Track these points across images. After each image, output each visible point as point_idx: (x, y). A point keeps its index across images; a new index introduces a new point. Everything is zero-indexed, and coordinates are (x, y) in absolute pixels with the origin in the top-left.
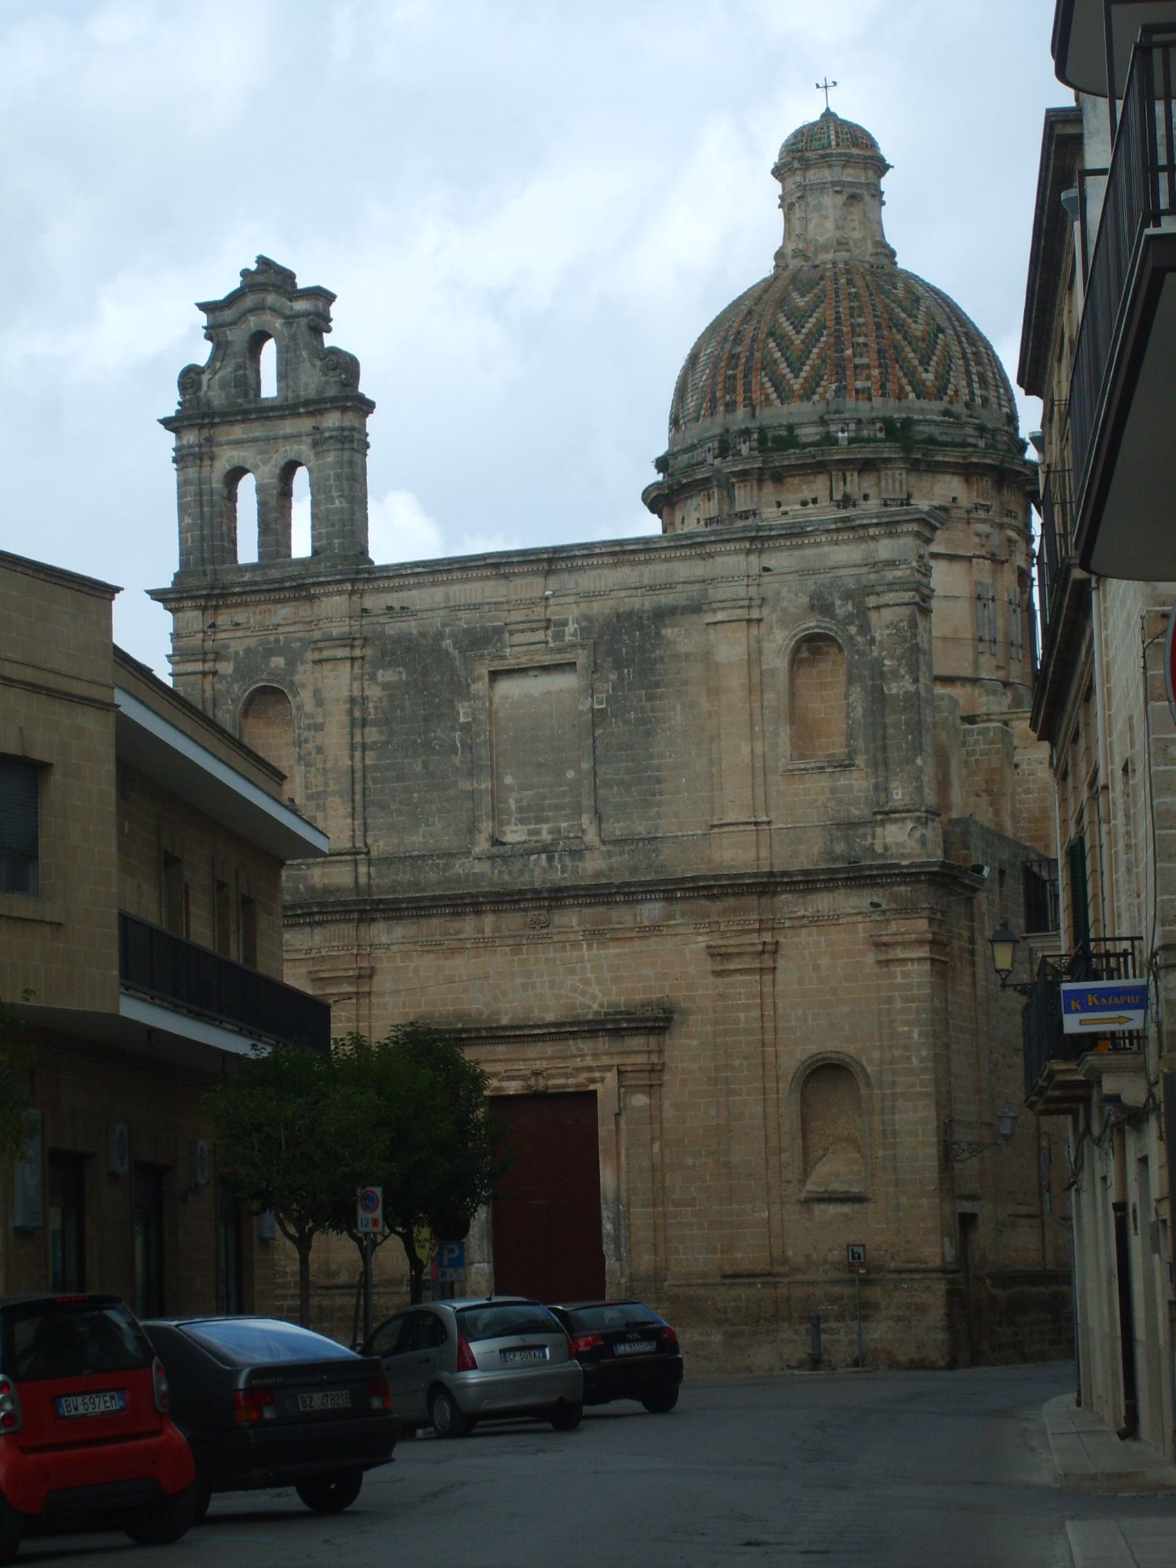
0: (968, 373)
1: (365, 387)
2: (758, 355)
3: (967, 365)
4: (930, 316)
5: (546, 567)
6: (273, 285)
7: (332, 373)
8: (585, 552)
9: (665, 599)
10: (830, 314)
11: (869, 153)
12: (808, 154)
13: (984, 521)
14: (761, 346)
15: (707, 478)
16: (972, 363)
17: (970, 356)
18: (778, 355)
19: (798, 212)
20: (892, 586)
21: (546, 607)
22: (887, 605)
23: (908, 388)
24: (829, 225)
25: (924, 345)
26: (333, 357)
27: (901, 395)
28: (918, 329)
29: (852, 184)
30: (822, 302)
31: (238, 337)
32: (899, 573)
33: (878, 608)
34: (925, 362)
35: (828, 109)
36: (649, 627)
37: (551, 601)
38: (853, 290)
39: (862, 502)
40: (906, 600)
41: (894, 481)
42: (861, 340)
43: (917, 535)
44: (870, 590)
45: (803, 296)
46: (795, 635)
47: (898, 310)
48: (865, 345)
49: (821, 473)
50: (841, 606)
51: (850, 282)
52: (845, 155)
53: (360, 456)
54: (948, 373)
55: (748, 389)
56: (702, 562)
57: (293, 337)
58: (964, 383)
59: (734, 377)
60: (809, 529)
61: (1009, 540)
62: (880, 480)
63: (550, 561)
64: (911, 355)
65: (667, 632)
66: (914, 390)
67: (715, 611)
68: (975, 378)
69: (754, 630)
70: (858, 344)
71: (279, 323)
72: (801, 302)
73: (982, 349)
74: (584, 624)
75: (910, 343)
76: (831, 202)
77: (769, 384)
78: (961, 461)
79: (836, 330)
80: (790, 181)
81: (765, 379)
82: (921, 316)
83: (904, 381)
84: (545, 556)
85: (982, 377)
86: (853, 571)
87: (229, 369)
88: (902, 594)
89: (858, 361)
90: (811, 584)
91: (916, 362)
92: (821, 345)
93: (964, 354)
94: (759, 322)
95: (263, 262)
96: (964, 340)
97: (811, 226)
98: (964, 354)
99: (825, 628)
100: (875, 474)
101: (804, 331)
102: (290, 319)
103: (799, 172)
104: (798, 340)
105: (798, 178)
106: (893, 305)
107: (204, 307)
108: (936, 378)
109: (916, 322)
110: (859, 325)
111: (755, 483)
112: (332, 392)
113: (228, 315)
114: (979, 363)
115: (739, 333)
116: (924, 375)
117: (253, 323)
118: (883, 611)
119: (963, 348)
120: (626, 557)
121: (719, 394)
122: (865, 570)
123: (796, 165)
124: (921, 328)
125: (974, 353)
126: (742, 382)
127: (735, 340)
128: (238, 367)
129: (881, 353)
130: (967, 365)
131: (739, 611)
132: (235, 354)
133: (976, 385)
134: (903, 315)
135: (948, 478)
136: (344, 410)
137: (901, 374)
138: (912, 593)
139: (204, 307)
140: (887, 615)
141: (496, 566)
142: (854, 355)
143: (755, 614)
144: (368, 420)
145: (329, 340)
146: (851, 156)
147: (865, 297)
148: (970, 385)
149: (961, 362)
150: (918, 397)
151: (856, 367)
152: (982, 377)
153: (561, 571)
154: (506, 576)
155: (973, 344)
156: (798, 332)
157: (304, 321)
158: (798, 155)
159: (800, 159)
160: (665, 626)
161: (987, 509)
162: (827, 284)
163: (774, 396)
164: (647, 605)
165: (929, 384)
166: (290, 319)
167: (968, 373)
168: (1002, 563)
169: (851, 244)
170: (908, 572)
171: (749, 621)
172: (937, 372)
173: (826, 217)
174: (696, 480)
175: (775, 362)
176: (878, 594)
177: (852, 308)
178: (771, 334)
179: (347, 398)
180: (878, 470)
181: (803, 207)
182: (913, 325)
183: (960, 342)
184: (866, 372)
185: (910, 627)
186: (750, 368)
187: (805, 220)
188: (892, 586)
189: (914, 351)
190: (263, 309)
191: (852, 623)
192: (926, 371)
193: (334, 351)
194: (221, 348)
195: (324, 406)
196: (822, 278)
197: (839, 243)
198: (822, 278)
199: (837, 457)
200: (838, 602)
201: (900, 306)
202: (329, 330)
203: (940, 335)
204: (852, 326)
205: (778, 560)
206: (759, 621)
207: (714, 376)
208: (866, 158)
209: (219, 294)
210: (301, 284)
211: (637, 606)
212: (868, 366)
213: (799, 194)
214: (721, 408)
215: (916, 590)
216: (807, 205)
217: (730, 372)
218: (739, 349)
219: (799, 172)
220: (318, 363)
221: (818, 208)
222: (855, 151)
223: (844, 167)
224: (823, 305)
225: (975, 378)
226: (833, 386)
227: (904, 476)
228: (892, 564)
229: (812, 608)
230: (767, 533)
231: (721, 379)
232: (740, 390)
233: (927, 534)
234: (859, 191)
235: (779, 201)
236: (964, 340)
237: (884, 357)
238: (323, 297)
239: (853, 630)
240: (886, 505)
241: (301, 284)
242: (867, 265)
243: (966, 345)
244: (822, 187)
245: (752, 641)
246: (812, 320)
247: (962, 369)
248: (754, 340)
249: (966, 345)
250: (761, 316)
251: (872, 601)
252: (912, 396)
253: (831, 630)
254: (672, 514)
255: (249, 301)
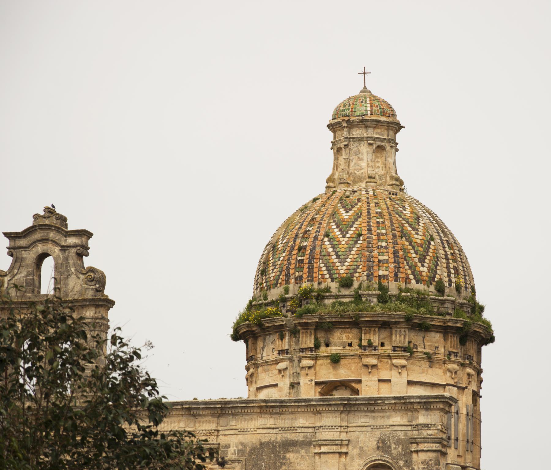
0: (448, 268)
1: (109, 292)
2: (318, 249)
3: (448, 263)
4: (426, 229)
5: (220, 412)
6: (55, 227)
7: (90, 283)
8: (244, 405)
9: (290, 436)
10: (365, 226)
11: (390, 120)
12: (352, 119)
13: (454, 362)
14: (320, 243)
15: (282, 325)
16: (451, 261)
17: (450, 257)
18: (331, 250)
19: (344, 154)
20: (426, 440)
21: (217, 436)
22: (423, 451)
23: (411, 277)
24: (364, 164)
25: (422, 249)
26: (92, 274)
27: (407, 280)
28: (418, 238)
29: (380, 139)
30: (360, 217)
31: (30, 256)
32: (430, 432)
33: (417, 452)
34: (422, 260)
35: (365, 87)
36: (280, 452)
37: (221, 433)
38: (381, 220)
39: (380, 348)
40: (434, 449)
41: (400, 335)
42: (384, 244)
43: (442, 410)
44: (413, 441)
45: (347, 212)
46: (367, 464)
47: (407, 225)
48: (386, 248)
49: (355, 328)
50: (395, 449)
51: (377, 204)
52: (376, 121)
53: (104, 334)
54: (436, 267)
55: (311, 270)
56: (313, 416)
57: (66, 259)
58: (446, 274)
59: (302, 261)
60: (379, 402)
61: (469, 375)
62: (391, 334)
63: (221, 408)
64: (414, 255)
65: (290, 456)
66: (415, 278)
67: (320, 446)
68: (452, 271)
69: (343, 459)
70: (382, 247)
71: (57, 249)
72: (346, 216)
73: (457, 252)
74: (240, 447)
75: (413, 248)
76: (365, 150)
77: (324, 269)
78: (442, 324)
79: (368, 238)
80: (339, 133)
81: (322, 265)
82: (421, 228)
83: (409, 272)
84: (219, 406)
85: (456, 269)
86: (404, 428)
87: (23, 275)
88: (431, 445)
89: (381, 258)
90: (378, 434)
91: (416, 260)
92: (358, 246)
93: (446, 255)
94: (319, 227)
95: (50, 211)
96: (446, 246)
97: (352, 164)
98: (446, 255)
99: (385, 461)
100: (388, 330)
101: (348, 236)
102: (64, 248)
103: (346, 129)
104: (344, 241)
105: (345, 133)
106: (404, 222)
107: (8, 235)
108: (429, 271)
109: (417, 234)
110: (383, 234)
111: (313, 331)
112: (90, 294)
113: (23, 242)
114: (455, 261)
115: (305, 232)
116: (422, 269)
117: (40, 248)
118: (420, 454)
119: (445, 251)
120: (268, 410)
121: (291, 272)
122: (410, 428)
123: (345, 124)
124: (420, 237)
125: (452, 254)
126: (307, 265)
127: (303, 237)
128: (28, 274)
129: (395, 254)
130: (448, 263)
131: (335, 447)
132: (27, 266)
133: (453, 276)
134: (410, 229)
135: (433, 334)
136: (97, 306)
137: (407, 267)
138: (437, 445)
139: (8, 235)
140: (423, 456)
141: (189, 409)
142: (379, 254)
143: (344, 450)
144: (109, 312)
145: (88, 262)
146: (379, 121)
147: (386, 213)
148: (449, 276)
149: (444, 261)
150: (417, 282)
151: (380, 261)
152: (456, 269)
153: (228, 414)
154: (194, 416)
155: (451, 248)
156: (344, 236)
157: (73, 250)
158: (346, 118)
159: (348, 122)
160: (289, 452)
161: (456, 354)
162: (362, 205)
163: (327, 276)
164: (279, 439)
165: (424, 274)
166: (64, 248)
167: (448, 268)
168: (464, 389)
169: (377, 177)
170: (436, 431)
171: (340, 454)
172: (429, 267)
173: (362, 159)
174: (275, 325)
175: (329, 255)
176: (417, 443)
177: (378, 222)
178: (327, 235)
179: (100, 300)
180: (391, 328)
181: (347, 151)
182: (416, 236)
183: (444, 248)
184: (386, 265)
185: (436, 464)
186: (313, 258)
187: (348, 161)
188: (426, 440)
189: (416, 253)
190: (47, 240)
191: (401, 459)
192: (423, 266)
193: (92, 270)
194: (17, 261)
195: (85, 303)
196: (359, 200)
197: (370, 177)
198: (359, 200)
199: (367, 319)
200: (393, 446)
201: (408, 222)
202: (87, 255)
203: (432, 243)
204: (379, 235)
205: (362, 420)
206: (346, 454)
207: (288, 259)
208: (389, 123)
209: (20, 229)
210: (72, 226)
211: (273, 439)
212: (387, 262)
213: (346, 143)
214: (293, 281)
215: (440, 443)
216: (350, 150)
217: (299, 258)
218: (305, 244)
219: (346, 129)
220: (82, 277)
221: (357, 153)
222: (383, 119)
223: (375, 128)
224: (360, 220)
225: (452, 271)
226: (365, 273)
227: (407, 332)
228: (426, 426)
229: (378, 448)
230: (354, 402)
231: (293, 262)
232: (306, 270)
233: (447, 409)
234: (383, 144)
235: (331, 145)
236: (446, 246)
237: (398, 257)
238: (86, 234)
239: (401, 463)
240: (394, 350)
241: (72, 226)
242: (387, 193)
243: (447, 249)
244: (361, 139)
245: (341, 466)
246: (353, 229)
247: (445, 265)
248: (316, 238)
249: (447, 249)
250: (320, 224)
251: (414, 447)
252: (413, 281)
253: (388, 462)
254: (255, 344)
255: (37, 236)
